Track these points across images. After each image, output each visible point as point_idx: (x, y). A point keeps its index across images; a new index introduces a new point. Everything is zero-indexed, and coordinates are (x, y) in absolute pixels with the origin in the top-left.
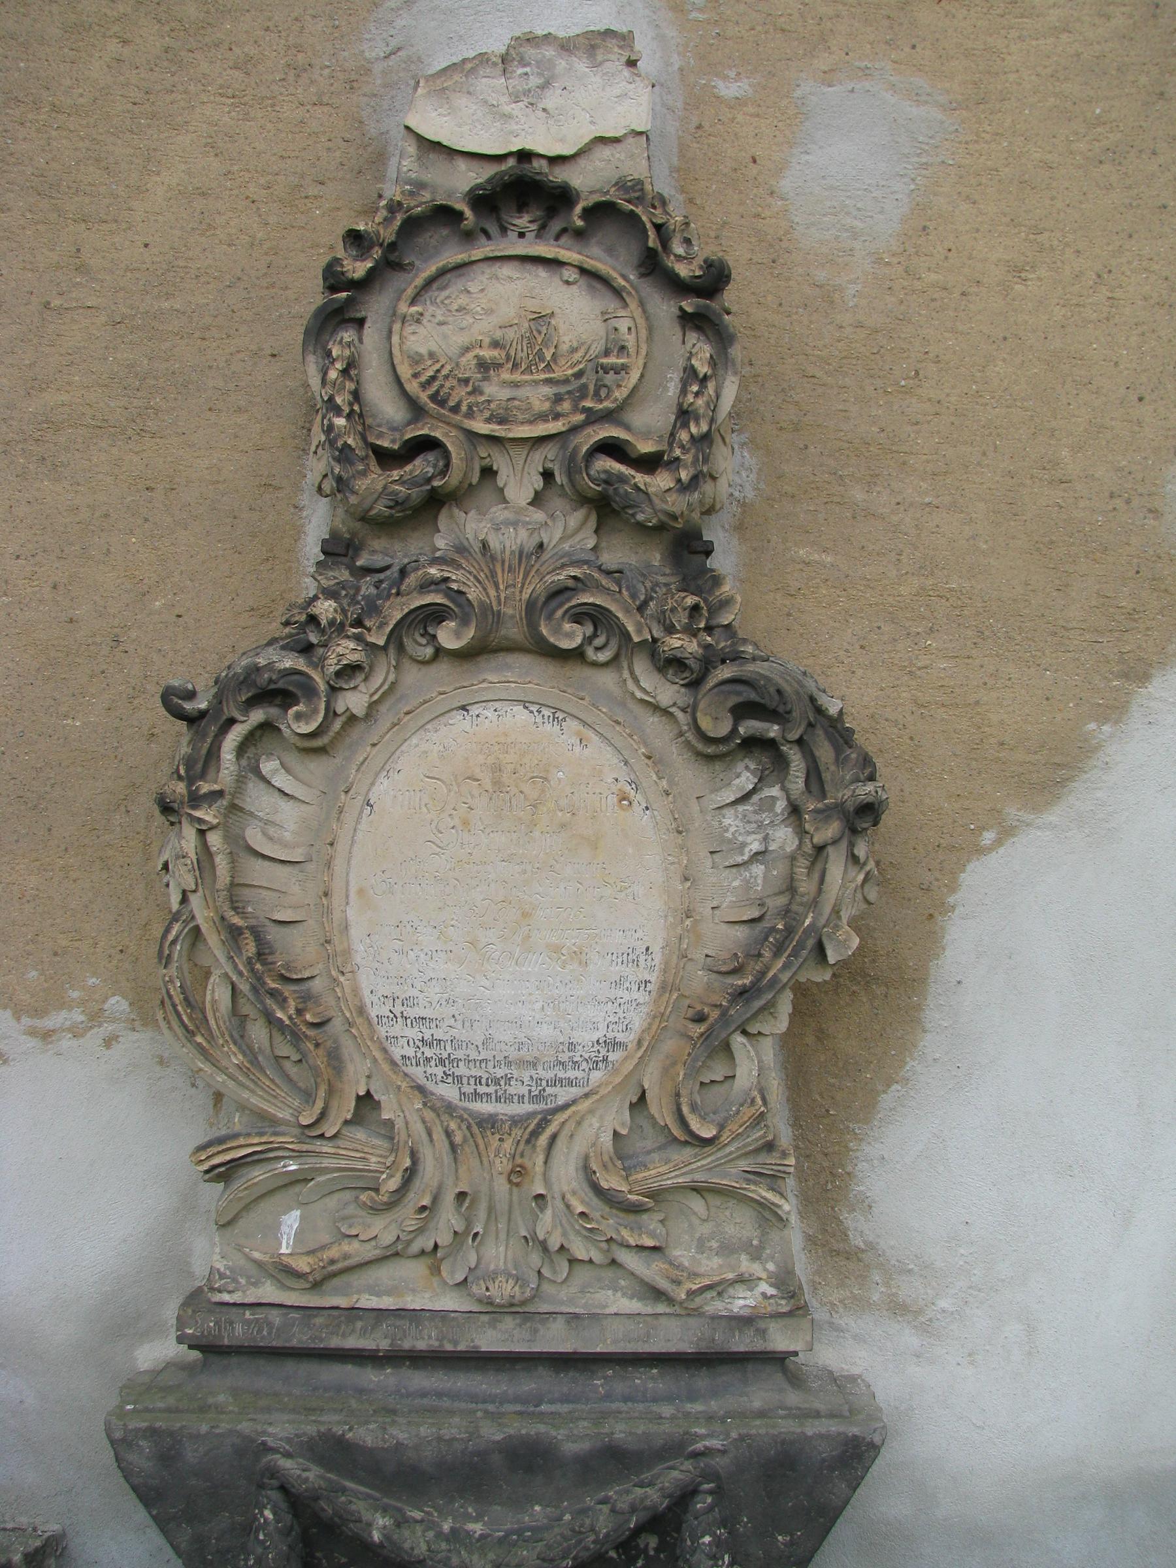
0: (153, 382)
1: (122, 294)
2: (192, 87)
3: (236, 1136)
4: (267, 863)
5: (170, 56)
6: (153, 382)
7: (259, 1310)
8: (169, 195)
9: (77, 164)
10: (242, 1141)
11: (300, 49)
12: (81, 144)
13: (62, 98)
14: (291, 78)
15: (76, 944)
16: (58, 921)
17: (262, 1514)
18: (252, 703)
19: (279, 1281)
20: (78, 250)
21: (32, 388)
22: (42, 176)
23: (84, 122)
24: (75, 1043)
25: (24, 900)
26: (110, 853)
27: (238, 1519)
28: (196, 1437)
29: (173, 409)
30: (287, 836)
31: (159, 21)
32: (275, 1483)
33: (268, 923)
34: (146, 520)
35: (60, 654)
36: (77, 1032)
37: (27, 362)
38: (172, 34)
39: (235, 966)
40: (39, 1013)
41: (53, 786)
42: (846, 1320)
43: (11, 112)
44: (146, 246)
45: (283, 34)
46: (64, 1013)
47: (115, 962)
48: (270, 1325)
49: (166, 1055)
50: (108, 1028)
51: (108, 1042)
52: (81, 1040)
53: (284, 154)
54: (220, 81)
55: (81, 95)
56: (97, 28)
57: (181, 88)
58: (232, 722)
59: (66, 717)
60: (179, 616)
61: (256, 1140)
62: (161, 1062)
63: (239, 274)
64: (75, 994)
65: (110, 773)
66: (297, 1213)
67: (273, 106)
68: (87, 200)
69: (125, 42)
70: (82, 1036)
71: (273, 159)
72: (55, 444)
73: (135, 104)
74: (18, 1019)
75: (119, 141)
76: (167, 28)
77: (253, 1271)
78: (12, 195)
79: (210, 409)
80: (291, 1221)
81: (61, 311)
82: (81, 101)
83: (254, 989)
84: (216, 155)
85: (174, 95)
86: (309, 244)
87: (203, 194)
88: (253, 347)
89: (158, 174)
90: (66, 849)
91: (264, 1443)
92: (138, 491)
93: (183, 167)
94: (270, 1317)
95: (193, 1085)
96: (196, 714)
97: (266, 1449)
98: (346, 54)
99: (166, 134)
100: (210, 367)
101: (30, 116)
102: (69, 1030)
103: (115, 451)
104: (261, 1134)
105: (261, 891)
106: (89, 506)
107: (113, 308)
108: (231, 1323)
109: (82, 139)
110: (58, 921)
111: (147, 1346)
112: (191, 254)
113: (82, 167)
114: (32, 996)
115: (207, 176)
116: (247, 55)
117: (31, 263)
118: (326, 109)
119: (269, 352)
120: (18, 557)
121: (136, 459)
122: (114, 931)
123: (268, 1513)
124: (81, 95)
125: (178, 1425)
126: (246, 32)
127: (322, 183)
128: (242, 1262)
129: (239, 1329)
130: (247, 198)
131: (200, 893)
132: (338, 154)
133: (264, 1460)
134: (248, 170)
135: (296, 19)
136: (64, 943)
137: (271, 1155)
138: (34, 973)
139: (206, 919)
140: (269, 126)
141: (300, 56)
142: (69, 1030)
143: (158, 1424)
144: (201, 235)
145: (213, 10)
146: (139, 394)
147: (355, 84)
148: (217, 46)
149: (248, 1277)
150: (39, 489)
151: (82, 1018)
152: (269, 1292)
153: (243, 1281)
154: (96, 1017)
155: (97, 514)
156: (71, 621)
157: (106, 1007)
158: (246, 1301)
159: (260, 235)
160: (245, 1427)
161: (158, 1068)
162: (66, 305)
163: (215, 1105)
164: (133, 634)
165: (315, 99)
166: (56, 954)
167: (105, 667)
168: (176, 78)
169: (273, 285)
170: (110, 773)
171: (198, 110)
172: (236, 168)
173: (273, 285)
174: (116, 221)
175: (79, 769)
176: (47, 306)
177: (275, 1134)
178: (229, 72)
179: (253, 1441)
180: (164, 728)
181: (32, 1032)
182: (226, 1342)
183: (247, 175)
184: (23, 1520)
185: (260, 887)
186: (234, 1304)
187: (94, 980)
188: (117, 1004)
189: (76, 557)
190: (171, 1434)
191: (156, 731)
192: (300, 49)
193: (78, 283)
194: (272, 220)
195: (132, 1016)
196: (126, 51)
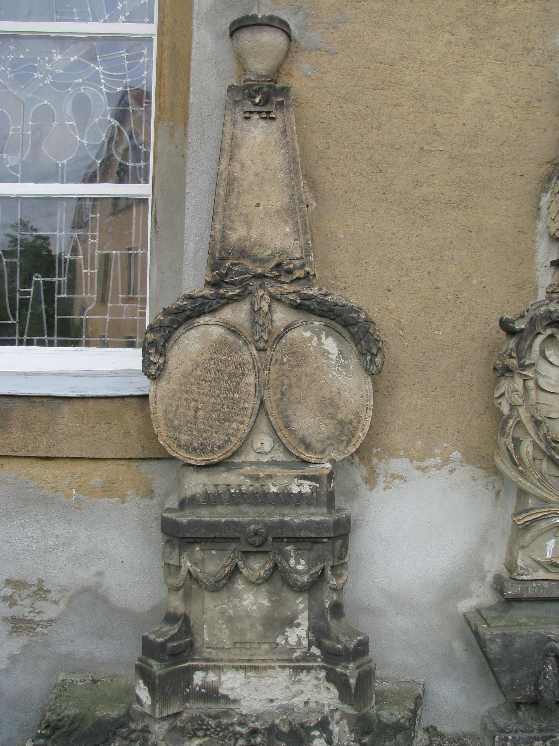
0: (470, 185)
1: (454, 145)
2: (482, 56)
3: (532, 509)
4: (544, 394)
5: (472, 41)
6: (470, 185)
7: (539, 582)
8: (473, 103)
9: (433, 86)
10: (537, 511)
11: (529, 41)
12: (434, 78)
13: (426, 58)
14: (526, 53)
15: (438, 429)
16: (431, 419)
17: (548, 667)
18: (549, 325)
19: (546, 569)
20: (435, 125)
21: (416, 185)
22: (417, 91)
23: (435, 69)
24: (437, 472)
25: (416, 410)
26: (455, 389)
27: (531, 670)
28: (522, 636)
29: (479, 197)
30: (552, 382)
31: (467, 26)
32: (553, 654)
33: (545, 418)
34: (469, 245)
35: (432, 303)
36: (437, 467)
37: (414, 173)
38: (473, 32)
39: (539, 437)
40: (421, 459)
41: (430, 360)
42: (498, 599)
43: (403, 63)
44: (464, 125)
45: (522, 34)
46: (432, 460)
47: (455, 437)
48: (543, 588)
49: (476, 476)
50: (451, 465)
51: (451, 471)
52: (440, 471)
53: (523, 87)
54: (495, 54)
55: (434, 57)
56: (440, 28)
57: (478, 56)
58: (539, 333)
59: (435, 330)
60: (485, 287)
61: (543, 510)
62: (474, 479)
63: (505, 139)
64: (438, 451)
65: (455, 355)
66: (553, 540)
67: (518, 65)
68: (437, 103)
69: (452, 34)
70: (440, 469)
71: (519, 89)
72: (427, 210)
73: (457, 62)
74: (412, 463)
75: (451, 78)
76: (471, 29)
77: (535, 565)
78: (404, 99)
79: (495, 198)
80: (551, 544)
81: (429, 152)
82: (434, 59)
83: (547, 447)
84: (494, 86)
85: (475, 59)
86: (535, 128)
87: (488, 103)
88: (513, 171)
89: (468, 93)
90: (436, 388)
91: (549, 638)
92: (464, 232)
93: (479, 91)
94: (544, 585)
95: (487, 489)
96: (519, 330)
97: (550, 639)
98: (548, 43)
99: (472, 76)
100: (494, 179)
101: (411, 65)
102: (434, 467)
103: (454, 214)
104: (545, 508)
105: (541, 405)
106: (443, 238)
107: (451, 151)
108: (527, 588)
109: (434, 76)
110: (431, 419)
111: (462, 602)
112: (484, 129)
113: (435, 88)
114: (419, 452)
115: (490, 95)
116: (506, 42)
117: (413, 130)
118: (541, 68)
119: (520, 174)
120: (412, 259)
121: (464, 218)
122: (456, 424)
123: (550, 667)
124: (434, 57)
125: (514, 632)
126: (506, 32)
127: (540, 101)
128: (530, 562)
129: (530, 590)
130: (508, 106)
131: (524, 407)
132: (546, 88)
133: (547, 645)
134: (508, 94)
135: (527, 27)
136: (433, 429)
137: (550, 516)
138: (420, 442)
139: (526, 418)
140: (516, 74)
141: (529, 44)
142: (434, 467)
143: (506, 632)
144: (488, 121)
145: (491, 22)
146: (465, 190)
147: (553, 57)
148: (493, 38)
149: (533, 569)
150: (421, 230)
151: (440, 461)
152: (541, 574)
153: (530, 570)
154: (446, 460)
155: (447, 242)
156: (437, 288)
157: (451, 456)
158: (533, 578)
159: (513, 122)
160: (541, 631)
161: (472, 482)
162: (431, 149)
163: (496, 497)
164: (464, 295)
165: (536, 63)
166: (429, 434)
167: (452, 308)
168: (475, 51)
169: (520, 145)
170: (455, 355)
171: (485, 66)
172: (503, 92)
173: (520, 145)
174: (451, 113)
175: (442, 353)
176: (422, 149)
177: (550, 507)
178: (499, 49)
179: (545, 637)
180: (478, 335)
181: (418, 468)
182: (525, 596)
183: (507, 96)
184: (408, 678)
185: (542, 404)
186: (528, 580)
187: (446, 445)
188: (456, 455)
189: (438, 260)
190: (511, 635)
191: (475, 337)
192: (529, 41)
193: (435, 140)
194: (519, 116)
195: (462, 460)
196: (453, 38)
